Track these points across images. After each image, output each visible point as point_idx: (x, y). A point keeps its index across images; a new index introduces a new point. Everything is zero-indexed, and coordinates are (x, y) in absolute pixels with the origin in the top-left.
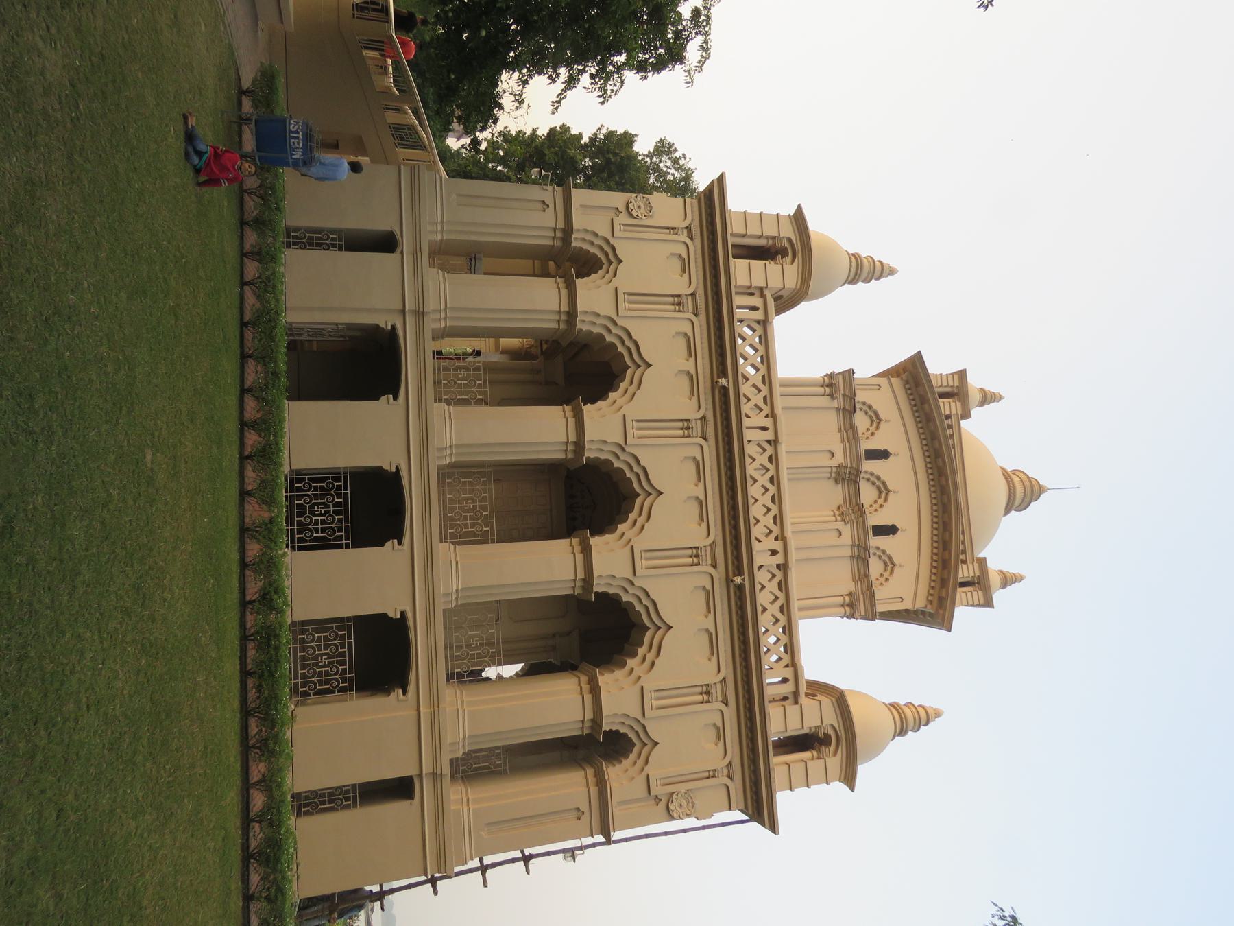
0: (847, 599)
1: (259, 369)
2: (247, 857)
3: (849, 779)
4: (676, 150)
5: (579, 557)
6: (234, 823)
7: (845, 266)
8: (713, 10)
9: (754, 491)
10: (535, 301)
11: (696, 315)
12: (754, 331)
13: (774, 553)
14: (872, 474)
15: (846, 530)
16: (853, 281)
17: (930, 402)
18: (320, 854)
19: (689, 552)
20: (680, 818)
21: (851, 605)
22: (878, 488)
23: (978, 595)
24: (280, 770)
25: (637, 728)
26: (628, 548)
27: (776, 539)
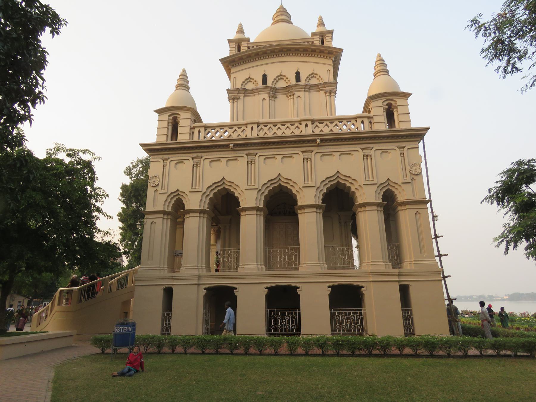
0: (327, 94)
2: (432, 356)
3: (406, 95)
4: (129, 167)
6: (417, 361)
7: (182, 92)
9: (279, 133)
10: (195, 227)
11: (202, 157)
12: (209, 132)
13: (307, 125)
14: (273, 82)
15: (297, 94)
16: (188, 88)
18: (431, 325)
19: (305, 162)
21: (330, 93)
22: (279, 79)
23: (328, 37)
26: (303, 189)
27: (301, 124)
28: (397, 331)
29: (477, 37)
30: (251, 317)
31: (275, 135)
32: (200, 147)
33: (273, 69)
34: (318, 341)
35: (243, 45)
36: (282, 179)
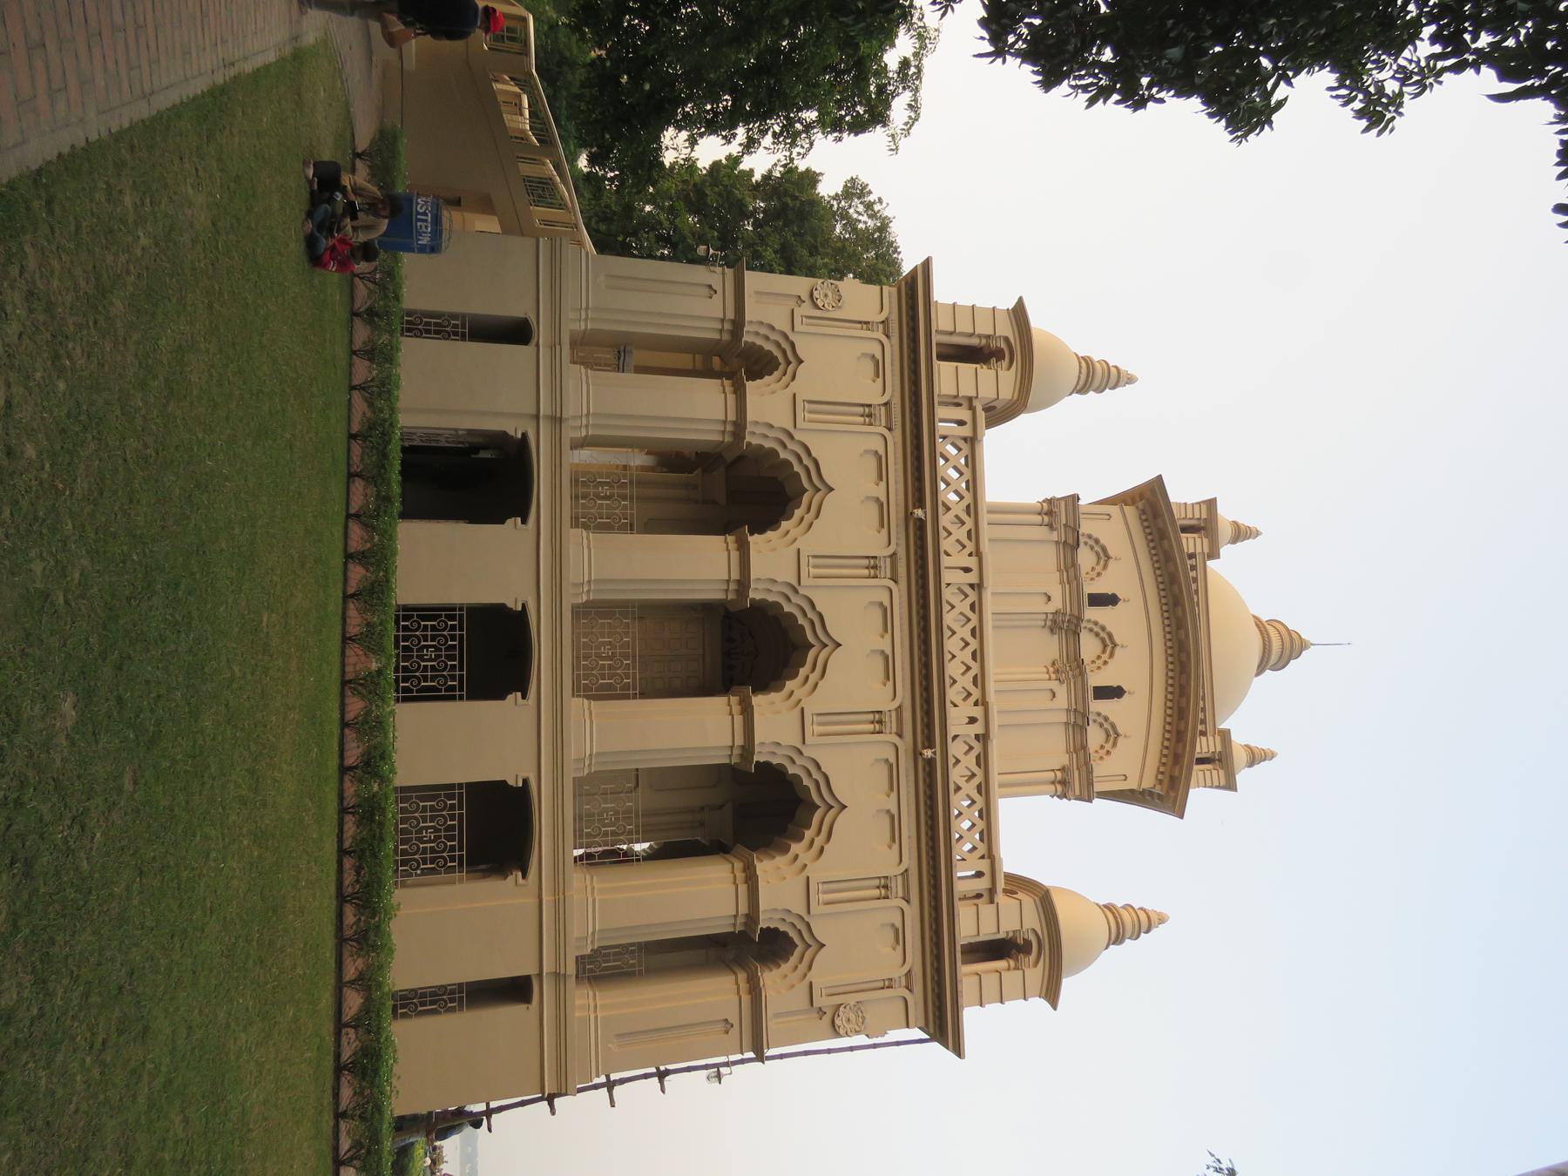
0: (1059, 774)
2: (339, 1069)
3: (1051, 994)
4: (870, 192)
6: (328, 1028)
7: (1072, 373)
9: (952, 645)
10: (695, 409)
11: (890, 429)
12: (959, 450)
13: (972, 720)
14: (1096, 623)
15: (1062, 691)
16: (1082, 389)
18: (420, 1064)
21: (1063, 783)
22: (1103, 640)
23: (1218, 775)
27: (976, 704)
28: (407, 969)
30: (447, 563)
31: (947, 633)
32: (917, 426)
34: (382, 757)
35: (1198, 541)
36: (825, 651)
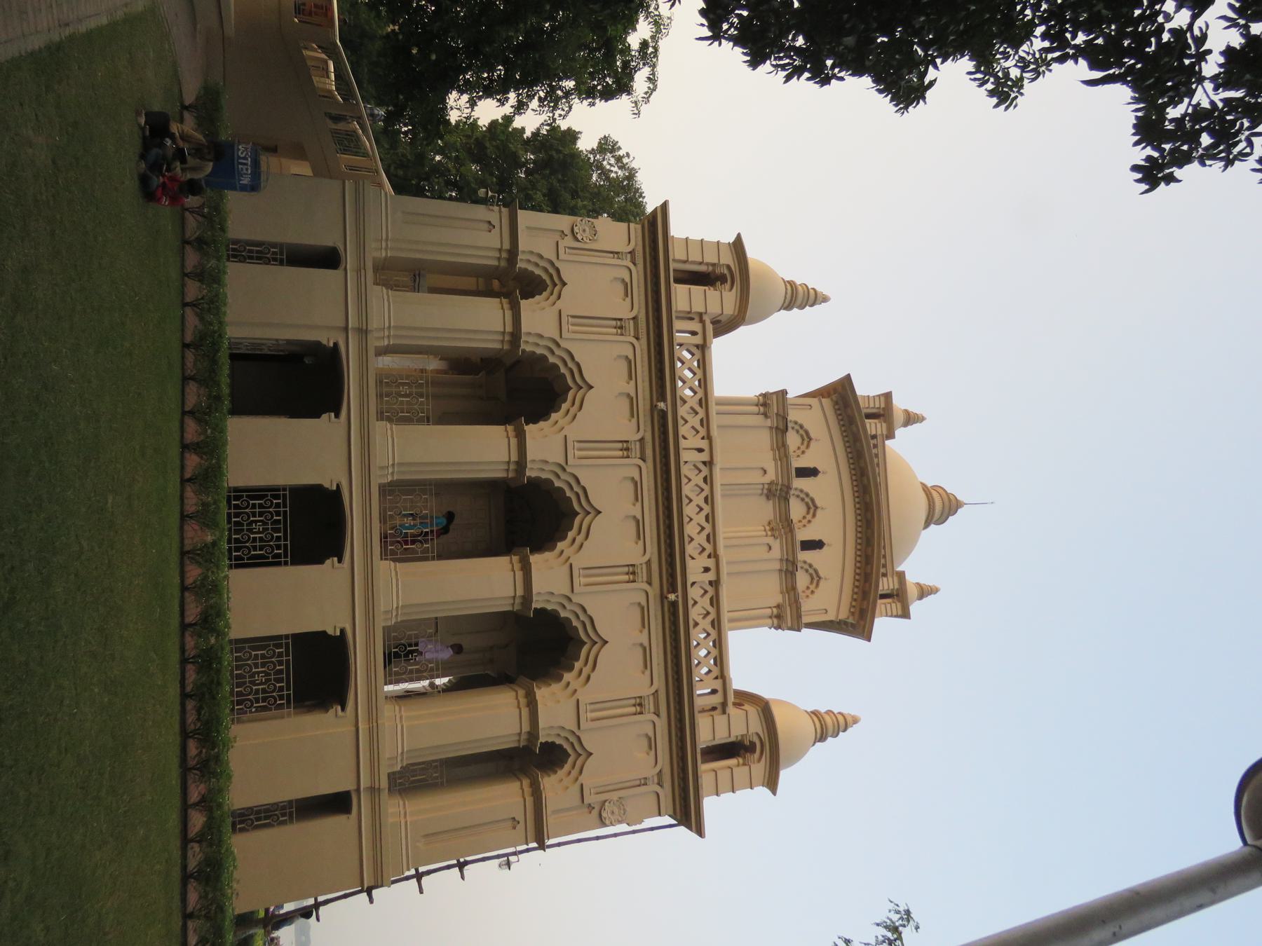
0: (775, 610)
1: (202, 392)
2: (186, 878)
3: (772, 783)
4: (619, 148)
5: (519, 574)
6: (176, 843)
7: (780, 293)
8: (661, 43)
9: (689, 510)
10: (479, 322)
11: (637, 339)
12: (693, 355)
13: (707, 570)
14: (801, 491)
15: (776, 545)
16: (788, 307)
17: (857, 421)
18: (256, 866)
19: (626, 569)
20: (612, 824)
21: (778, 617)
22: (807, 504)
24: (220, 791)
25: (572, 739)
26: (566, 567)
27: (709, 556)
28: (243, 791)
29: (878, 925)
31: (685, 501)
33: (830, 492)
36: (582, 392)
